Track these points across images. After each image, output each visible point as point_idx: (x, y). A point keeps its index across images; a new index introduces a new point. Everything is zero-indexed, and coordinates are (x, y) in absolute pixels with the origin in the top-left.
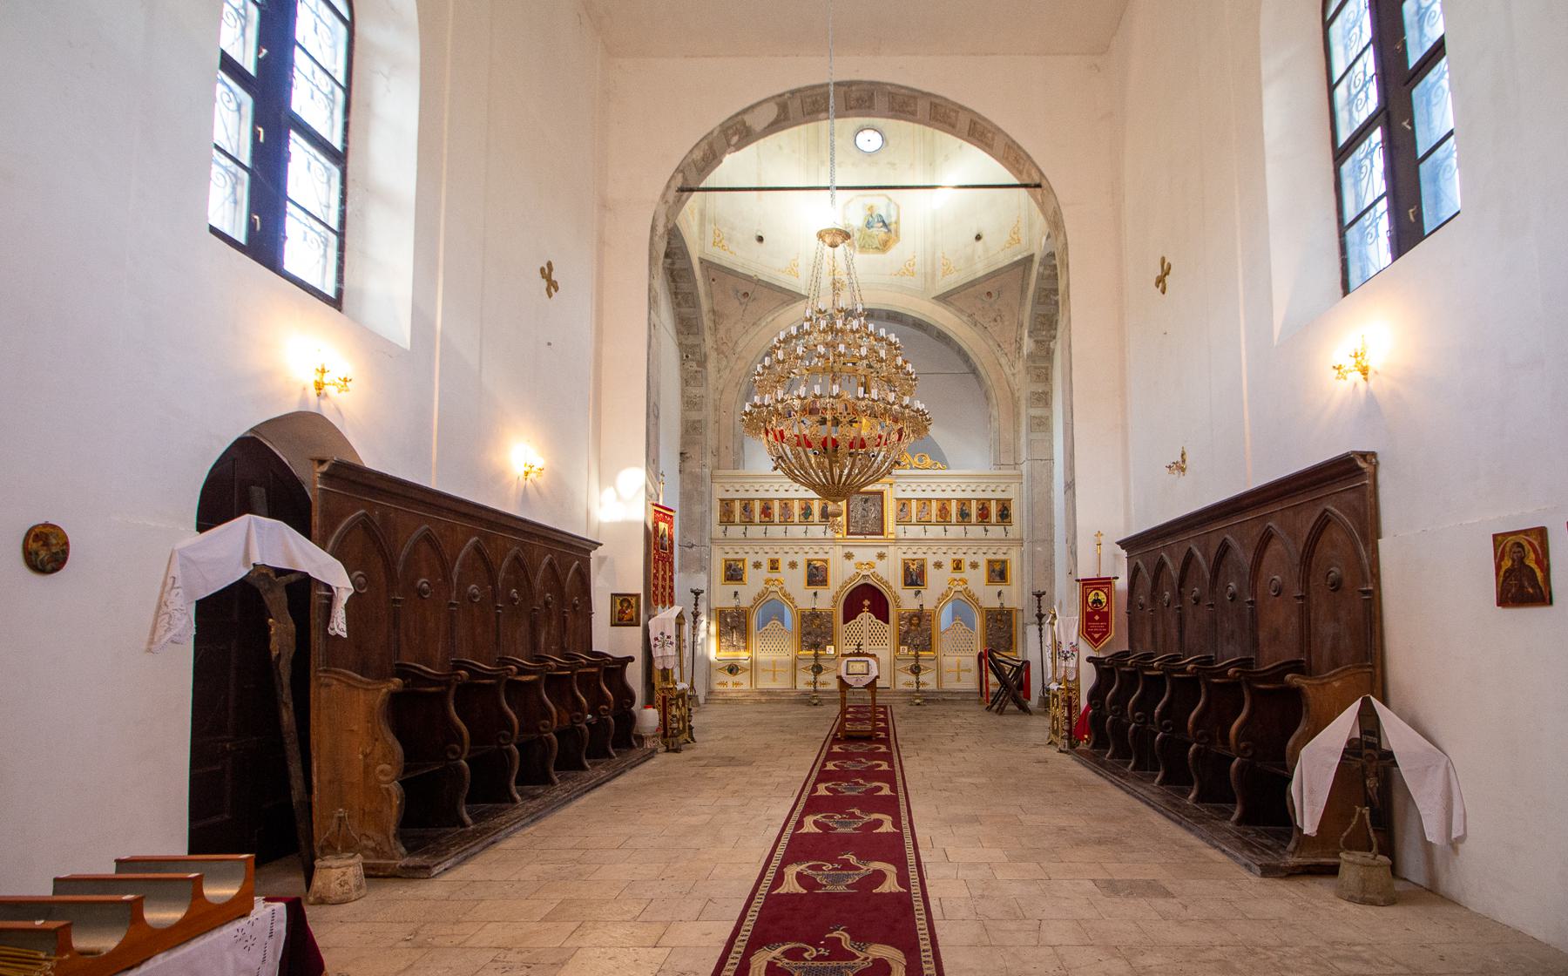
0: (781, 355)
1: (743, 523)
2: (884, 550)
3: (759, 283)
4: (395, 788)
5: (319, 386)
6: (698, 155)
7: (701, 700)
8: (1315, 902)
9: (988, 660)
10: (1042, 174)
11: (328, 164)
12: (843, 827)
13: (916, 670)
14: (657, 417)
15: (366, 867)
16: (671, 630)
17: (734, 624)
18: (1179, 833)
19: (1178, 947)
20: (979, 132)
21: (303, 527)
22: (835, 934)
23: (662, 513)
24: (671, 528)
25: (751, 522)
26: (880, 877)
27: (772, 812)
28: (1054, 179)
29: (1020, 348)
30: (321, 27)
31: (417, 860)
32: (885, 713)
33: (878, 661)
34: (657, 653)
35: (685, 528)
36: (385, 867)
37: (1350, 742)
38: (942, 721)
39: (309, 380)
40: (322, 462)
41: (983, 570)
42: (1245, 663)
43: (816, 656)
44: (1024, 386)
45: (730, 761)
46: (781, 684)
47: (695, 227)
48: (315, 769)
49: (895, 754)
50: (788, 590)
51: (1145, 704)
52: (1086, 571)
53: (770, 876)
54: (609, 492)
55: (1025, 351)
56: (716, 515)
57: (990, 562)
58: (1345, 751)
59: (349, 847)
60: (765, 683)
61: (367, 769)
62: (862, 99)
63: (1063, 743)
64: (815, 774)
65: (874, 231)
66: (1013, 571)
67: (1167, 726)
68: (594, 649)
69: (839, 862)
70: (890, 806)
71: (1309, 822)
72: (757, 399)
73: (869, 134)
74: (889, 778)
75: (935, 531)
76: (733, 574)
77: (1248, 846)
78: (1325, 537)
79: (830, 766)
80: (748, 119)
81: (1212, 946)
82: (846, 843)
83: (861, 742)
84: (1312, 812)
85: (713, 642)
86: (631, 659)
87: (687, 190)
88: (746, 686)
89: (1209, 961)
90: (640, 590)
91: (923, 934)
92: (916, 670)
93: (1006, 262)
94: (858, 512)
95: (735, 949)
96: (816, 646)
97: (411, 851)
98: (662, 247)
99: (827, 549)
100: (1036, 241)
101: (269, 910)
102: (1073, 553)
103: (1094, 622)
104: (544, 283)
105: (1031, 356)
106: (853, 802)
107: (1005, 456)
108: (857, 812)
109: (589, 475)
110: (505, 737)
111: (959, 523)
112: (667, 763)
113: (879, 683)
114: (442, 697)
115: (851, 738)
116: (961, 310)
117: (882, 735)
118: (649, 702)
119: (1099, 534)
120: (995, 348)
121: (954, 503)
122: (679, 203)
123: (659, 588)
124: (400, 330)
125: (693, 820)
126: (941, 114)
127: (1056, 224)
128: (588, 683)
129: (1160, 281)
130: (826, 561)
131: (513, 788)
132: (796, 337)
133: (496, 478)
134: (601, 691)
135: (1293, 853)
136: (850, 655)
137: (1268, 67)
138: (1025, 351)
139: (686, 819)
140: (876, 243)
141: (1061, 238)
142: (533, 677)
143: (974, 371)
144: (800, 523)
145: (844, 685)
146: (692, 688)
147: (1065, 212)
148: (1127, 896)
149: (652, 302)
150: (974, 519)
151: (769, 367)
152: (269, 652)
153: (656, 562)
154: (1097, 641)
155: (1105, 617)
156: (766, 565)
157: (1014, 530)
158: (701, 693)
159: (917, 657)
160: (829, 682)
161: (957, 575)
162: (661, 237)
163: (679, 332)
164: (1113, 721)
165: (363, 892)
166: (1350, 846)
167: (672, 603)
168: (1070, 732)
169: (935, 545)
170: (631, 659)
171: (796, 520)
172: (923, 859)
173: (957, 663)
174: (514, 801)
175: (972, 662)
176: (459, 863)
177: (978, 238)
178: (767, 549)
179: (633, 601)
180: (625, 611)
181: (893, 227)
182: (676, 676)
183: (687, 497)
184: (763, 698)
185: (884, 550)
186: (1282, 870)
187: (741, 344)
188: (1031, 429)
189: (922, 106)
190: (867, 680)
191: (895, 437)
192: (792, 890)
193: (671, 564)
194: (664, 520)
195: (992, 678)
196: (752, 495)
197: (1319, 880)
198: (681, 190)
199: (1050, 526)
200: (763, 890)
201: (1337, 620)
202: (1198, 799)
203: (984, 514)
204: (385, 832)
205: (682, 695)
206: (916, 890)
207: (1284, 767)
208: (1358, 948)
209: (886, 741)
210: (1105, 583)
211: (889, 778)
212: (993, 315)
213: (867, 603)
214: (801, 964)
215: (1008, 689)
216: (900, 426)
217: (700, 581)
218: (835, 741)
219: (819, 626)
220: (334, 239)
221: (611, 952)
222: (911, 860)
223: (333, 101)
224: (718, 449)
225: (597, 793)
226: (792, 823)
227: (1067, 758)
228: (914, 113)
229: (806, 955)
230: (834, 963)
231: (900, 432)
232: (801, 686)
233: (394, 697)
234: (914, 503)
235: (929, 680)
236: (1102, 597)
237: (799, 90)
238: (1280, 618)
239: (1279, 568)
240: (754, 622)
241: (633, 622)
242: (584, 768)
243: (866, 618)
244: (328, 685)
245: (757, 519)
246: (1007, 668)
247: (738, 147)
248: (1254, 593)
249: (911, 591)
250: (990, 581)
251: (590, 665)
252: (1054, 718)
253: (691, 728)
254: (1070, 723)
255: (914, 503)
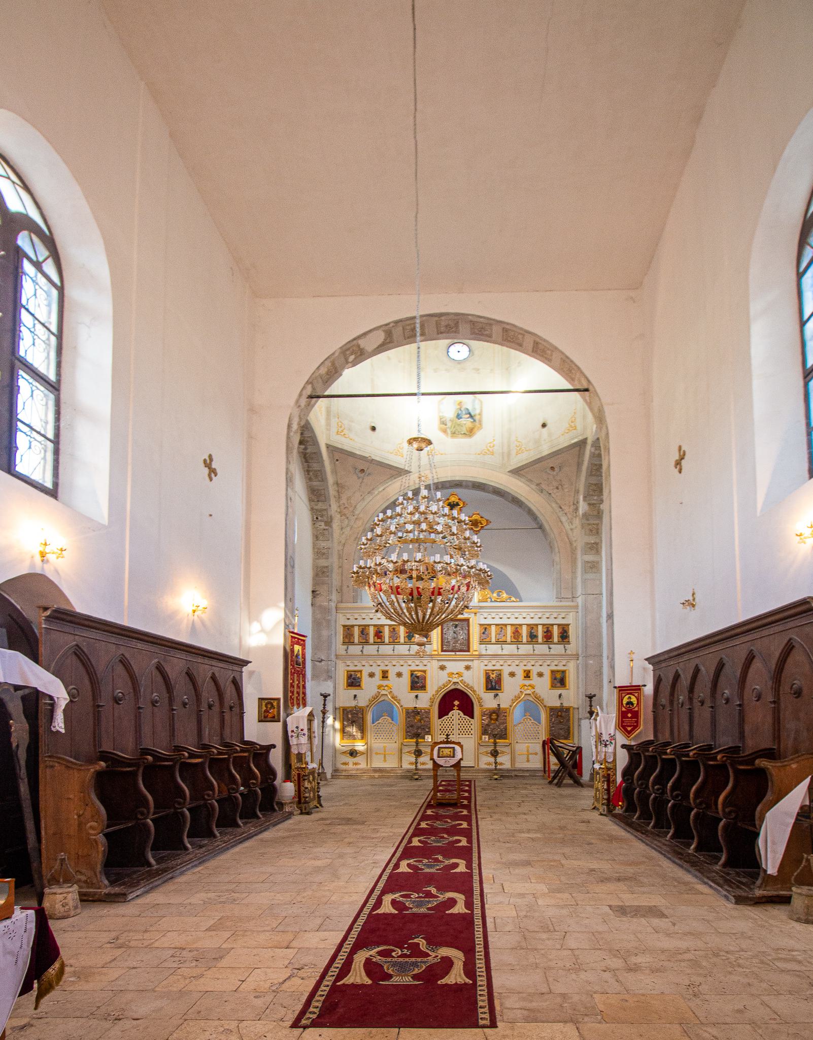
0: (378, 531)
1: (360, 643)
2: (469, 663)
3: (372, 461)
4: (101, 838)
5: (43, 555)
6: (323, 371)
7: (329, 776)
8: (771, 921)
9: (549, 745)
10: (589, 381)
11: (46, 392)
12: (427, 867)
13: (495, 754)
14: (293, 567)
15: (81, 894)
16: (304, 725)
17: (353, 717)
18: (680, 873)
19: (663, 951)
20: (540, 350)
21: (35, 657)
22: (416, 941)
23: (296, 638)
24: (304, 649)
25: (367, 642)
26: (452, 902)
27: (377, 857)
28: (598, 384)
29: (577, 509)
30: (39, 291)
31: (117, 890)
32: (469, 786)
33: (461, 747)
34: (293, 741)
35: (315, 648)
36: (95, 894)
37: (802, 808)
38: (512, 792)
39: (36, 550)
40: (46, 609)
41: (547, 678)
42: (735, 750)
43: (417, 743)
44: (580, 538)
45: (348, 821)
46: (391, 763)
47: (323, 421)
48: (43, 825)
49: (474, 816)
50: (396, 694)
51: (661, 780)
52: (622, 680)
53: (372, 902)
54: (255, 626)
55: (581, 511)
56: (340, 638)
57: (552, 672)
58: (798, 814)
59: (68, 880)
60: (378, 763)
61: (80, 825)
62: (448, 326)
63: (603, 809)
64: (411, 831)
65: (462, 421)
66: (571, 679)
67: (677, 796)
68: (247, 738)
69: (423, 892)
70: (466, 854)
71: (771, 866)
72: (362, 563)
73: (458, 347)
74: (467, 833)
75: (509, 649)
76: (353, 681)
77: (728, 882)
78: (790, 660)
79: (423, 825)
80: (362, 343)
81: (688, 950)
82: (430, 879)
83: (448, 808)
84: (774, 858)
85: (338, 736)
86: (274, 746)
87: (314, 397)
88: (363, 765)
89: (684, 961)
90: (280, 695)
91: (479, 940)
92: (495, 754)
93: (566, 444)
94: (450, 635)
95: (344, 950)
96: (417, 736)
97: (112, 883)
98: (296, 439)
99: (425, 662)
100: (590, 430)
101: (24, 914)
102: (612, 667)
103: (628, 718)
104: (206, 470)
105: (585, 515)
106: (439, 850)
107: (566, 592)
108: (440, 857)
109: (239, 611)
110: (179, 803)
111: (528, 643)
112: (300, 822)
113: (463, 764)
114: (134, 774)
115: (441, 805)
116: (530, 481)
117: (465, 802)
118: (288, 778)
119: (632, 653)
120: (558, 510)
121: (524, 628)
122: (309, 407)
123: (295, 693)
124: (101, 512)
125: (318, 863)
126: (512, 337)
127: (600, 419)
128: (241, 764)
129: (678, 464)
130: (424, 672)
131: (186, 840)
132: (391, 518)
133: (172, 616)
134: (251, 769)
135: (760, 887)
136: (441, 743)
137: (756, 307)
138: (581, 511)
139: (313, 862)
140: (464, 430)
141: (604, 428)
142: (200, 760)
143: (541, 527)
144: (405, 643)
145: (436, 766)
146: (321, 764)
147: (606, 409)
148: (632, 917)
149: (289, 480)
150: (540, 639)
151: (371, 540)
152: (11, 744)
153: (292, 674)
154: (629, 732)
155: (636, 715)
156: (378, 675)
157: (572, 648)
158: (329, 772)
159: (495, 744)
160: (426, 762)
161: (527, 682)
162: (296, 432)
163: (311, 500)
164: (639, 792)
165: (79, 911)
166: (800, 882)
167: (305, 705)
168: (608, 800)
169: (509, 659)
170: (274, 746)
171: (402, 640)
172: (485, 891)
173: (526, 750)
174: (186, 849)
175: (538, 748)
176: (147, 892)
177: (544, 425)
178: (379, 663)
179: (275, 704)
180: (269, 711)
181: (477, 418)
182: (308, 759)
183: (317, 624)
184: (376, 775)
185: (469, 663)
186: (751, 899)
187: (359, 508)
188: (585, 571)
189: (496, 330)
190: (453, 761)
191: (464, 589)
192: (388, 911)
193: (304, 676)
194: (298, 644)
195: (553, 760)
196: (367, 622)
197: (778, 907)
198: (311, 397)
199: (600, 645)
200: (366, 911)
201: (798, 719)
202: (697, 849)
203: (548, 636)
204: (93, 869)
205: (312, 772)
206: (477, 911)
207: (754, 826)
208: (794, 953)
209: (468, 807)
210: (635, 689)
211: (467, 833)
212: (555, 484)
213: (456, 703)
214: (389, 959)
215: (566, 767)
216: (468, 580)
217: (327, 687)
218: (429, 806)
219: (420, 721)
220: (50, 446)
221: (255, 951)
222: (477, 891)
223: (49, 345)
224: (341, 590)
225: (247, 844)
226: (391, 866)
227: (606, 820)
228: (490, 336)
229: (393, 954)
230: (413, 959)
231: (468, 585)
232: (406, 766)
233: (99, 775)
234: (493, 628)
235: (505, 761)
236: (634, 700)
237: (401, 321)
238: (759, 716)
239: (759, 678)
240: (369, 717)
241: (275, 719)
242: (238, 826)
243: (456, 714)
244: (52, 767)
245: (371, 640)
246: (566, 752)
247: (355, 363)
248: (741, 697)
249: (491, 694)
250: (553, 686)
251: (243, 751)
252: (597, 790)
253: (319, 797)
254: (609, 793)
255: (493, 628)
